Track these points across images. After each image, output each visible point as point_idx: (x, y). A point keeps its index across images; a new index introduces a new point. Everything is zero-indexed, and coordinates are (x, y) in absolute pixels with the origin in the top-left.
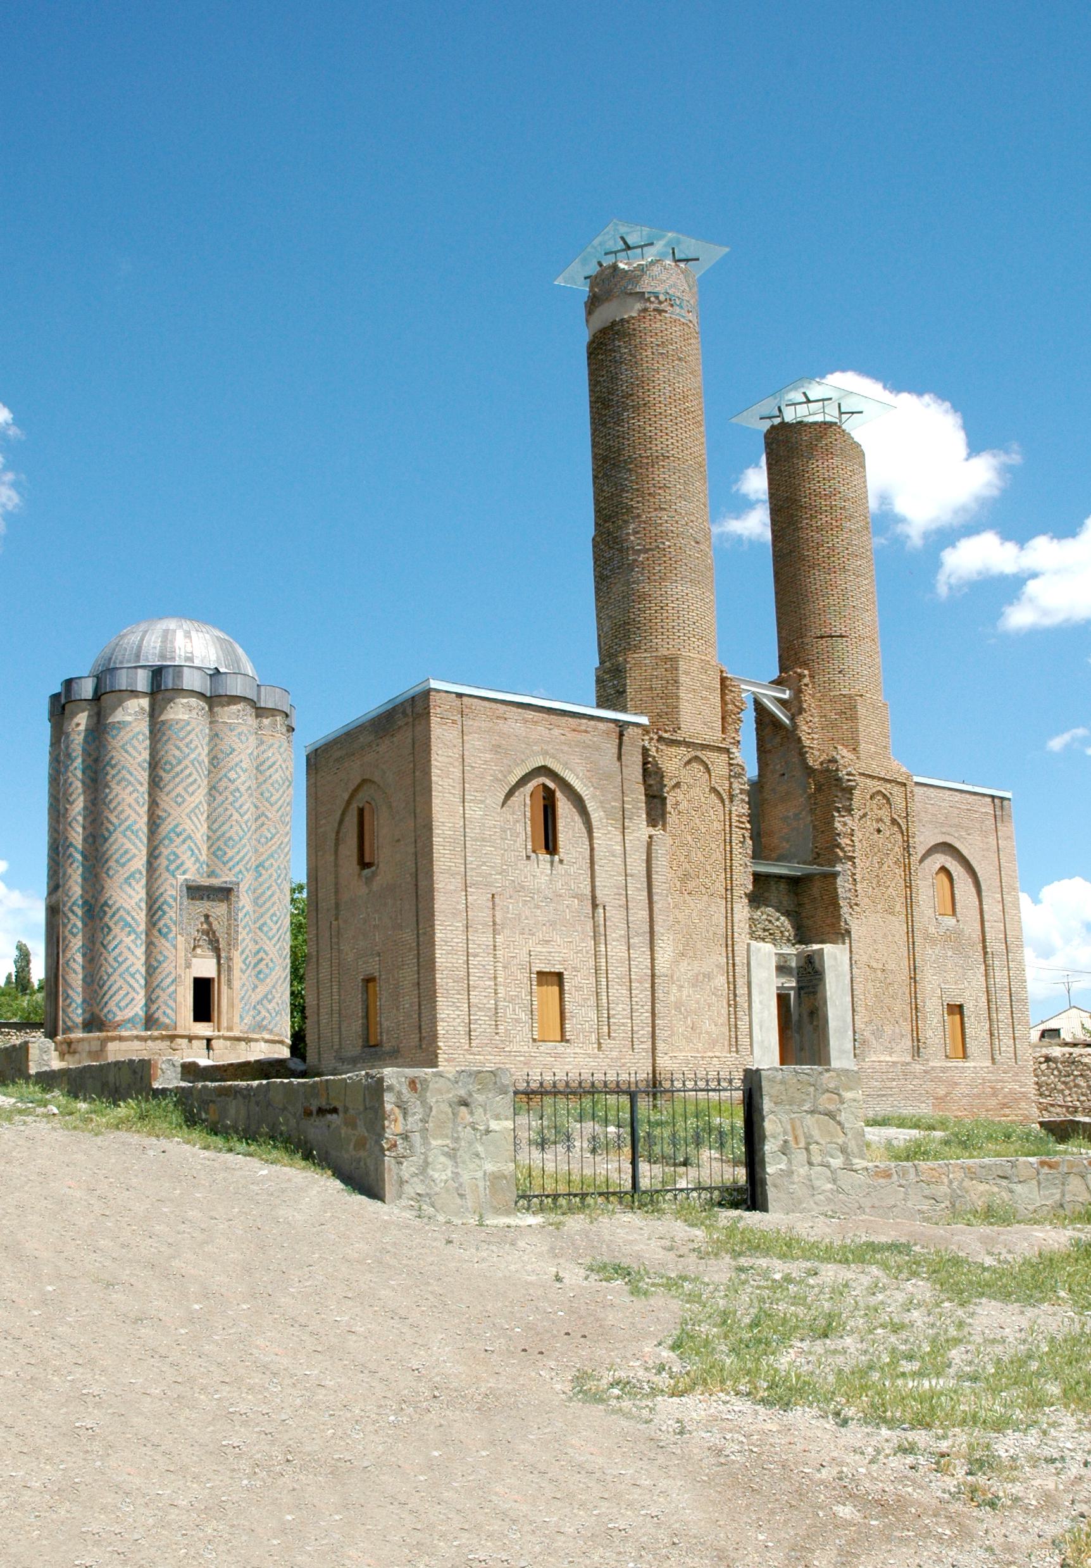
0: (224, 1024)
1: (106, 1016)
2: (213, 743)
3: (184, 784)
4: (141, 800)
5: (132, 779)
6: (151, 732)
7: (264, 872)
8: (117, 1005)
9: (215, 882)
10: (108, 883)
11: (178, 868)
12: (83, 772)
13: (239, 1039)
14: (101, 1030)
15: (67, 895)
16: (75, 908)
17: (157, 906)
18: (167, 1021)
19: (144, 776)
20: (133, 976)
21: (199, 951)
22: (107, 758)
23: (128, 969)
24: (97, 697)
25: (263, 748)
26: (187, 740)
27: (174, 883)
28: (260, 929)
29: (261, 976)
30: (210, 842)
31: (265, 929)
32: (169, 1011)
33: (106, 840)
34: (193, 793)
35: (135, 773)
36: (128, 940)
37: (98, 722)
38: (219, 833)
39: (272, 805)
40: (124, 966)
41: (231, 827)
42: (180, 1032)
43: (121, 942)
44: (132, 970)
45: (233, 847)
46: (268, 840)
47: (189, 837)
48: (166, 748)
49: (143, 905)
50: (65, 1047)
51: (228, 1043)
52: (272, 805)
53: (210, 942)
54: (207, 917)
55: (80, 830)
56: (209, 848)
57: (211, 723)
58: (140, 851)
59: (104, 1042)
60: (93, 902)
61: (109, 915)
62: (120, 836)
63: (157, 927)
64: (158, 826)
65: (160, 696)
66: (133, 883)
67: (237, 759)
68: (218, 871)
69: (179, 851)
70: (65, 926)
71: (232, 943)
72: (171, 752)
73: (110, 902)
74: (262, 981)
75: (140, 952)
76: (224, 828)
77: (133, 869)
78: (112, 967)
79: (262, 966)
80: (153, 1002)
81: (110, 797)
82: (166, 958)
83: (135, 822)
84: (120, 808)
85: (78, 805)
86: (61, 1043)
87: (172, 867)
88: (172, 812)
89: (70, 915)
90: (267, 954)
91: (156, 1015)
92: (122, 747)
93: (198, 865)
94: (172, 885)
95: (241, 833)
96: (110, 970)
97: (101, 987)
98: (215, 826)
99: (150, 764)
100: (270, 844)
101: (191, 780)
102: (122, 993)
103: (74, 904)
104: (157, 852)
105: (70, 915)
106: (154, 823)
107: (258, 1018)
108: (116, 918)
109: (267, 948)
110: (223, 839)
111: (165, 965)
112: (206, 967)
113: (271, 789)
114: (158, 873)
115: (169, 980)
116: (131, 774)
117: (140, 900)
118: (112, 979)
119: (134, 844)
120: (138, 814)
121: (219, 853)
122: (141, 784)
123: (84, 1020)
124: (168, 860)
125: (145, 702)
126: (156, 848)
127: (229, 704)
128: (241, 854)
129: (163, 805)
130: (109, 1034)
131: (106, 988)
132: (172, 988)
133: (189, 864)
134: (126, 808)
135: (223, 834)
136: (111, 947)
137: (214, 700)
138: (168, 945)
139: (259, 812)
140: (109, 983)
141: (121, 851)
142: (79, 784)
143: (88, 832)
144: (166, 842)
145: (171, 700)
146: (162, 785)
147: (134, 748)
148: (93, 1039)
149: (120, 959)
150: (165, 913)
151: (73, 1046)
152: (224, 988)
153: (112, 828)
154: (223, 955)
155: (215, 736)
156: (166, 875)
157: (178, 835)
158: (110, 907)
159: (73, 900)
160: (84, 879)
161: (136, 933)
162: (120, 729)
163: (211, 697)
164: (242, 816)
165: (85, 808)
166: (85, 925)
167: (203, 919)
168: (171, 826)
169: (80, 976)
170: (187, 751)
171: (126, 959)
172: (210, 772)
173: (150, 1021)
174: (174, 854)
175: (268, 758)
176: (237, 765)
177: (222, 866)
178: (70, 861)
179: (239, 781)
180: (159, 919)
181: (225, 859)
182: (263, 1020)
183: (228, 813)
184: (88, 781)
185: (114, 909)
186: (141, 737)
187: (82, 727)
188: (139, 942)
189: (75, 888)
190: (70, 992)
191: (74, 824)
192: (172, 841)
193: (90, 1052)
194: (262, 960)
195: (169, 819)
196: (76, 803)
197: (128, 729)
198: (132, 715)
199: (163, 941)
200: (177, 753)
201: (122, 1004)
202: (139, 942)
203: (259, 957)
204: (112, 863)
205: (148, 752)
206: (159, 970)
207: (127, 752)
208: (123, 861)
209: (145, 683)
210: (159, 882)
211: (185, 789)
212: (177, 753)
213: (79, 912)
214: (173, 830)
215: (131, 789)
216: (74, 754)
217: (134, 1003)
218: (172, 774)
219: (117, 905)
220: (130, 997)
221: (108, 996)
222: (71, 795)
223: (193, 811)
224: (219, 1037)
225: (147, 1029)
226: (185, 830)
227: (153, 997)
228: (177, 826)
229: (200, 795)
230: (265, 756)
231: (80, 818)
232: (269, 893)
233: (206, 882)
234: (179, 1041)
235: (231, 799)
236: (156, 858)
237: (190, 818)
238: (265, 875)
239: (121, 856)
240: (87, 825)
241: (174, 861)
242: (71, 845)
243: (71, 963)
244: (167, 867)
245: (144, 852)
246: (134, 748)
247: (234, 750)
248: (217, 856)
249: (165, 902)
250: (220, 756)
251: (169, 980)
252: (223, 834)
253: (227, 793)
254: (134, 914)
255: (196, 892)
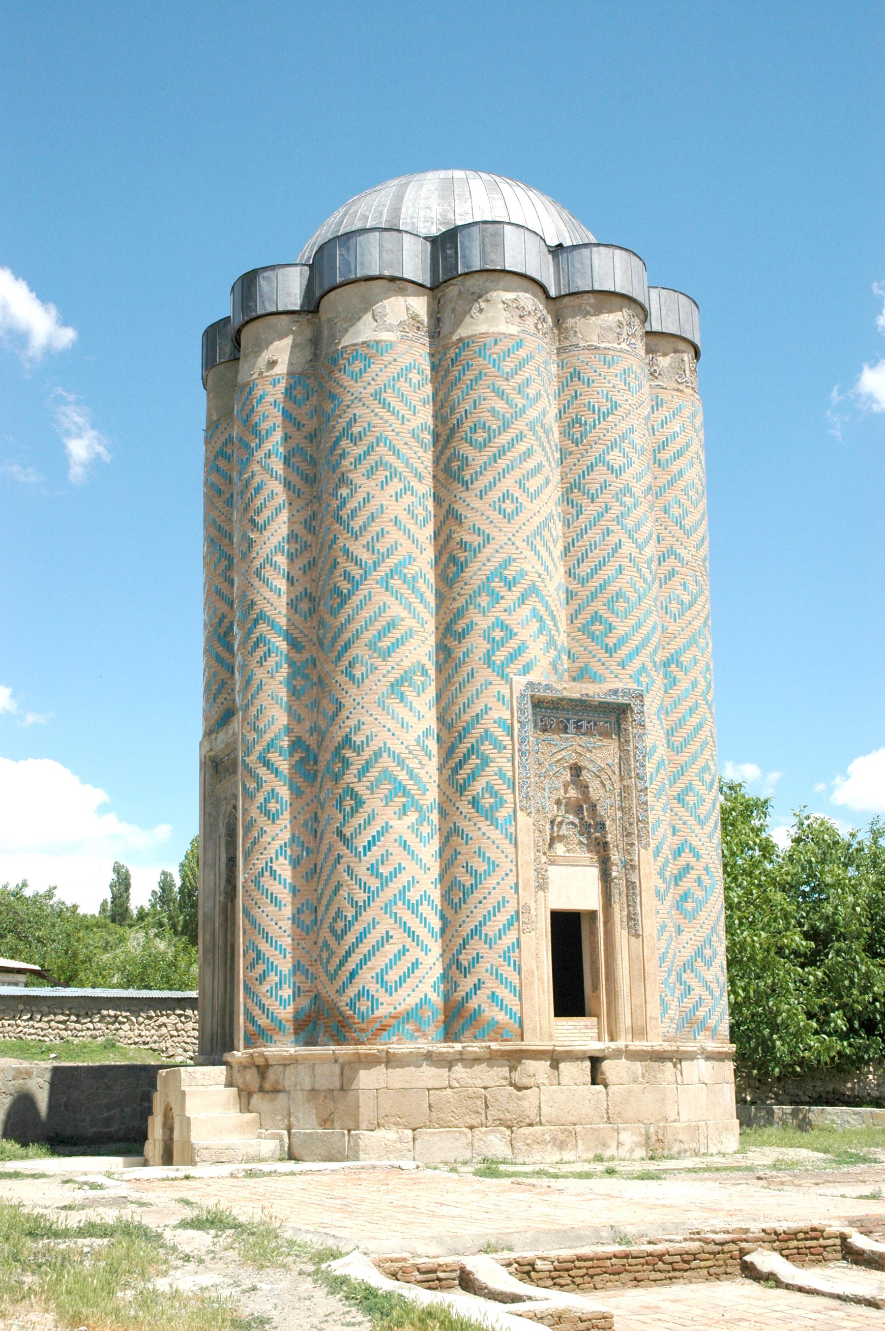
0: (625, 1020)
1: (352, 1005)
2: (569, 393)
3: (517, 473)
4: (419, 511)
5: (398, 464)
6: (434, 368)
7: (680, 675)
8: (380, 979)
9: (595, 691)
10: (351, 695)
11: (512, 657)
12: (287, 461)
13: (659, 1057)
14: (340, 1040)
15: (255, 729)
16: (274, 757)
17: (463, 748)
18: (501, 1017)
19: (424, 460)
20: (413, 908)
21: (560, 849)
22: (343, 422)
23: (403, 891)
24: (312, 305)
25: (662, 413)
26: (519, 379)
27: (506, 691)
28: (680, 799)
29: (689, 906)
30: (574, 604)
31: (691, 799)
32: (503, 993)
33: (344, 599)
34: (538, 492)
35: (405, 451)
36: (401, 826)
37: (316, 357)
38: (593, 584)
39: (688, 534)
40: (394, 887)
41: (620, 570)
42: (532, 1042)
43: (386, 829)
44: (413, 895)
45: (627, 614)
46: (685, 607)
47: (533, 590)
48: (474, 395)
49: (432, 745)
50: (251, 1077)
51: (638, 1066)
52: (688, 534)
53: (585, 829)
54: (576, 770)
55: (281, 584)
56: (572, 619)
57: (560, 351)
58: (423, 623)
59: (348, 1071)
60: (312, 741)
61: (353, 770)
62: (377, 589)
63: (469, 794)
64: (462, 567)
65: (452, 290)
66: (410, 694)
67: (624, 426)
68: (595, 667)
69: (512, 621)
70: (249, 796)
71: (634, 829)
72: (486, 404)
73: (358, 739)
74: (692, 916)
75: (429, 851)
76: (603, 574)
77: (407, 664)
78: (365, 888)
79: (688, 883)
80: (465, 972)
81: (352, 505)
82: (494, 865)
83: (411, 559)
84: (374, 528)
85: (277, 530)
86: (244, 1067)
87: (500, 656)
88: (494, 533)
89: (262, 771)
90: (697, 856)
91: (473, 1004)
92: (376, 395)
93: (553, 653)
94: (500, 698)
95: (640, 584)
96: (361, 896)
97: (340, 937)
98: (584, 569)
99: (436, 436)
100: (689, 615)
101: (530, 464)
102: (390, 949)
103: (270, 746)
104: (461, 624)
105: (262, 771)
106: (450, 562)
107: (688, 1003)
108: (373, 773)
109: (695, 843)
110: (603, 598)
111: (491, 882)
112: (576, 887)
113: (684, 500)
114: (465, 670)
115: (502, 918)
116: (397, 453)
117: (427, 733)
118: (366, 917)
119: (409, 607)
120: (415, 541)
121: (597, 628)
122: (420, 478)
123: (297, 1013)
124: (491, 641)
125: (419, 305)
126: (459, 614)
127: (598, 311)
128: (644, 630)
129: (471, 518)
130: (363, 1049)
131: (350, 938)
132: (510, 938)
133: (534, 652)
134: (390, 527)
135: (602, 587)
136: (361, 842)
137: (565, 305)
138: (495, 834)
139: (663, 547)
140: (358, 927)
141: (378, 625)
142: (278, 488)
143: (299, 588)
144: (484, 600)
145: (478, 296)
146: (467, 475)
147: (402, 398)
148: (323, 1060)
149: (384, 870)
150: (486, 761)
151: (271, 1076)
152: (621, 935)
153: (356, 572)
154: (615, 857)
155: (571, 379)
156: (485, 674)
157: (510, 585)
158: (358, 750)
159: (268, 737)
160: (294, 692)
161: (419, 809)
162: (367, 359)
163: (560, 297)
164: (640, 548)
165: (292, 537)
166: (297, 792)
167: (567, 776)
168: (491, 566)
169: (288, 911)
170: (520, 402)
171: (399, 869)
172: (564, 454)
173: (456, 1018)
174: (504, 627)
175: (675, 435)
176: (623, 438)
177: (603, 656)
178: (260, 652)
179: (631, 471)
180: (473, 776)
181: (611, 641)
182: (696, 1007)
183: (613, 539)
184: (295, 479)
185: (367, 754)
186: (415, 377)
187: (281, 368)
188: (426, 830)
189: (273, 708)
190: (263, 947)
191: (268, 572)
192: (497, 598)
193: (313, 1091)
194: (688, 868)
195: (488, 550)
196: (273, 526)
197: (387, 358)
198: (393, 327)
199: (484, 825)
200: (500, 405)
201: (392, 977)
202: (426, 830)
203: (682, 861)
204: (359, 650)
205: (430, 409)
206: (478, 895)
207: (385, 405)
208: (385, 643)
209: (418, 260)
210: (470, 690)
211: (521, 484)
212: (500, 405)
213: (284, 766)
214: (498, 574)
215: (396, 485)
216: (265, 426)
217: (418, 973)
218: (490, 451)
219: (375, 745)
220: (409, 958)
221: (355, 959)
222: (259, 512)
223: (538, 532)
224: (617, 1054)
225: (449, 1036)
226: (523, 574)
227: (465, 959)
228: (507, 563)
229: (546, 504)
230: (667, 431)
231: (282, 560)
232: (694, 721)
233: (574, 691)
234: (531, 1065)
235: (616, 509)
236: (461, 636)
237: (533, 548)
238: (684, 684)
239: (381, 635)
240: (297, 574)
241: (503, 642)
242: (261, 617)
243: (266, 881)
244: (488, 655)
245: (431, 626)
246: (402, 398)
247: (615, 406)
248: (592, 636)
249: (486, 735)
250: (589, 418)
251: (502, 918)
252: (602, 587)
253: (606, 497)
254: (413, 764)
255: (553, 713)
